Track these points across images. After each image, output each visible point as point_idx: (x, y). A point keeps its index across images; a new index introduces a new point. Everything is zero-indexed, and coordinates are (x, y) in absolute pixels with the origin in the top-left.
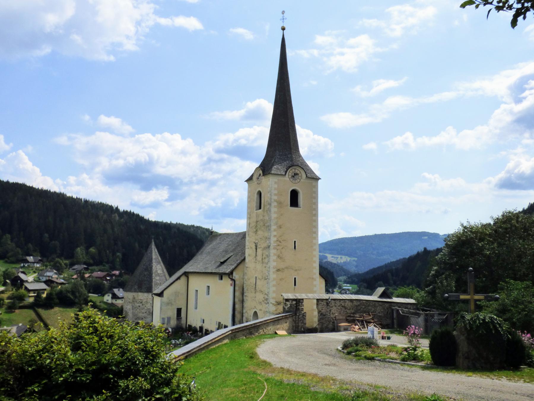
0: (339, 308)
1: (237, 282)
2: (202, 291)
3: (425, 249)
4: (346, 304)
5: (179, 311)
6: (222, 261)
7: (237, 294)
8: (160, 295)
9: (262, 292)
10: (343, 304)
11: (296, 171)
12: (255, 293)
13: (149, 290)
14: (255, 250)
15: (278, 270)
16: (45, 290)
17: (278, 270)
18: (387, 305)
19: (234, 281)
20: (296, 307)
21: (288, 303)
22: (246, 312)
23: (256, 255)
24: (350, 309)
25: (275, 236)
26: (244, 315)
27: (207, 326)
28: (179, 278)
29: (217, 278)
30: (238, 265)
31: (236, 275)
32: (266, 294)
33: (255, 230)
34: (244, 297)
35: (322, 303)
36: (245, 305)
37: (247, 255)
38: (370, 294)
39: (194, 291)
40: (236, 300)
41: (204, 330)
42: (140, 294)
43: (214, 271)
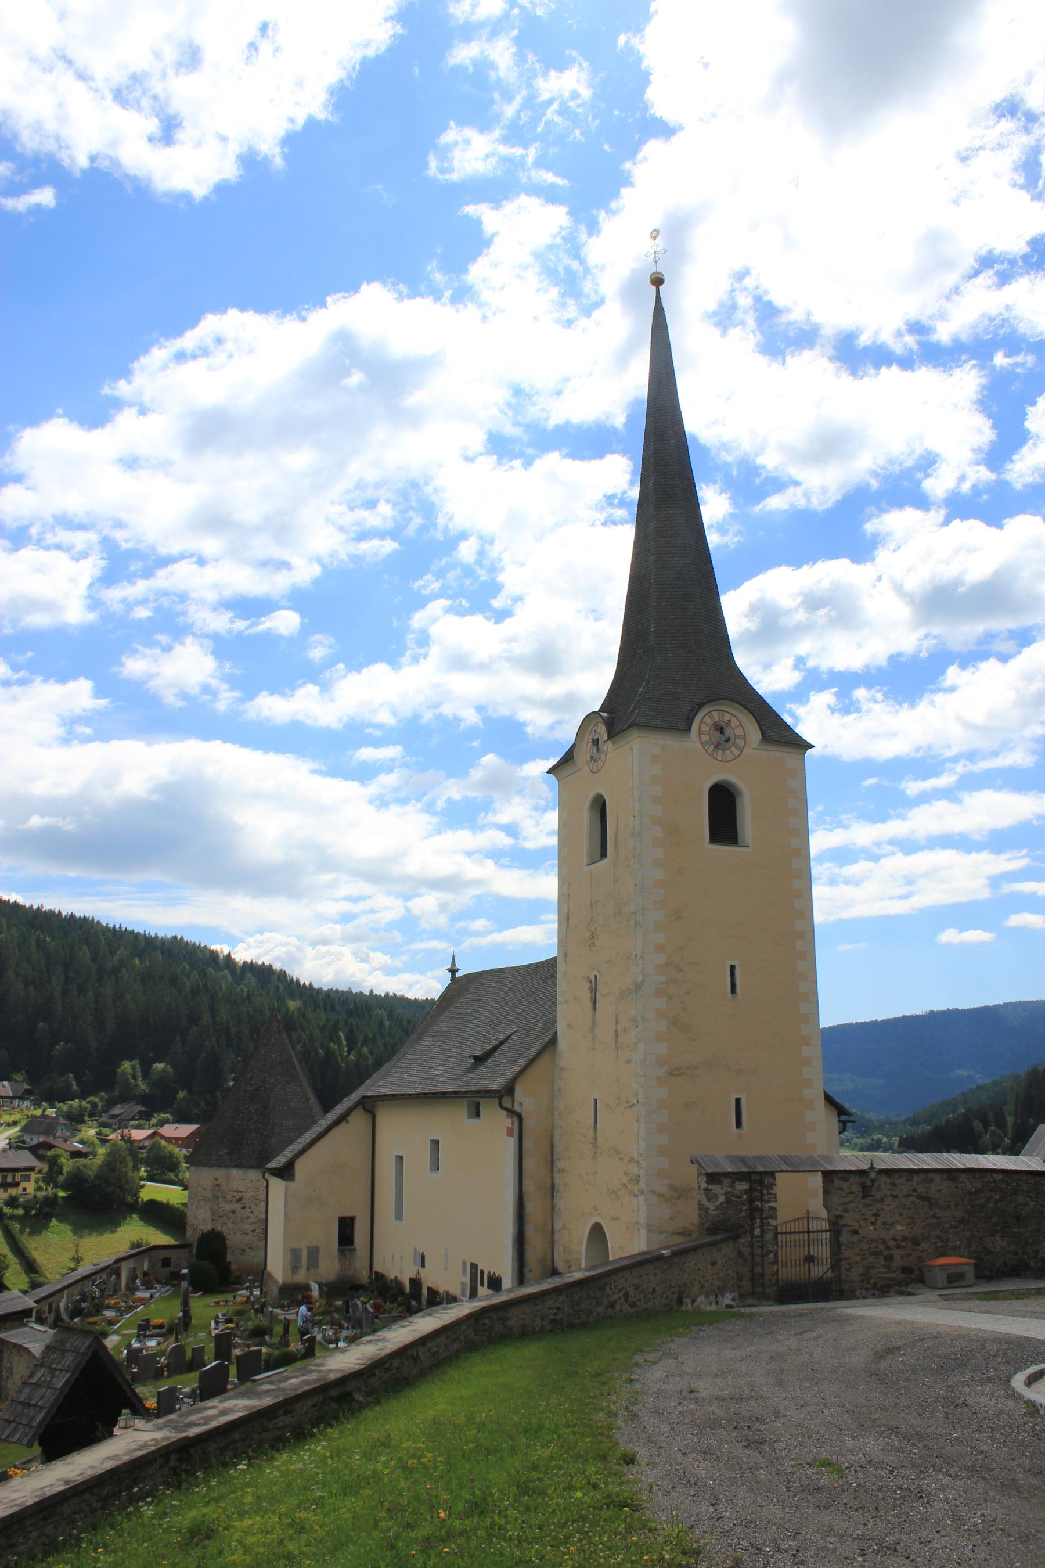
1: (528, 1123)
2: (418, 1158)
5: (346, 1226)
6: (478, 1052)
8: (286, 1172)
9: (617, 1152)
10: (921, 1189)
11: (727, 717)
12: (595, 1157)
13: (260, 1162)
14: (589, 1005)
17: (675, 1072)
19: (520, 1117)
20: (751, 1200)
21: (715, 1188)
22: (564, 1227)
23: (594, 1024)
24: (948, 1207)
25: (659, 948)
26: (557, 1236)
27: (434, 1278)
28: (343, 1118)
29: (460, 1112)
30: (532, 1061)
31: (524, 1098)
32: (631, 1160)
33: (588, 935)
34: (557, 1175)
35: (845, 1185)
36: (560, 1204)
37: (561, 1027)
38: (1014, 1150)
39: (393, 1160)
40: (529, 1186)
41: (425, 1291)
42: (235, 1172)
43: (451, 1089)
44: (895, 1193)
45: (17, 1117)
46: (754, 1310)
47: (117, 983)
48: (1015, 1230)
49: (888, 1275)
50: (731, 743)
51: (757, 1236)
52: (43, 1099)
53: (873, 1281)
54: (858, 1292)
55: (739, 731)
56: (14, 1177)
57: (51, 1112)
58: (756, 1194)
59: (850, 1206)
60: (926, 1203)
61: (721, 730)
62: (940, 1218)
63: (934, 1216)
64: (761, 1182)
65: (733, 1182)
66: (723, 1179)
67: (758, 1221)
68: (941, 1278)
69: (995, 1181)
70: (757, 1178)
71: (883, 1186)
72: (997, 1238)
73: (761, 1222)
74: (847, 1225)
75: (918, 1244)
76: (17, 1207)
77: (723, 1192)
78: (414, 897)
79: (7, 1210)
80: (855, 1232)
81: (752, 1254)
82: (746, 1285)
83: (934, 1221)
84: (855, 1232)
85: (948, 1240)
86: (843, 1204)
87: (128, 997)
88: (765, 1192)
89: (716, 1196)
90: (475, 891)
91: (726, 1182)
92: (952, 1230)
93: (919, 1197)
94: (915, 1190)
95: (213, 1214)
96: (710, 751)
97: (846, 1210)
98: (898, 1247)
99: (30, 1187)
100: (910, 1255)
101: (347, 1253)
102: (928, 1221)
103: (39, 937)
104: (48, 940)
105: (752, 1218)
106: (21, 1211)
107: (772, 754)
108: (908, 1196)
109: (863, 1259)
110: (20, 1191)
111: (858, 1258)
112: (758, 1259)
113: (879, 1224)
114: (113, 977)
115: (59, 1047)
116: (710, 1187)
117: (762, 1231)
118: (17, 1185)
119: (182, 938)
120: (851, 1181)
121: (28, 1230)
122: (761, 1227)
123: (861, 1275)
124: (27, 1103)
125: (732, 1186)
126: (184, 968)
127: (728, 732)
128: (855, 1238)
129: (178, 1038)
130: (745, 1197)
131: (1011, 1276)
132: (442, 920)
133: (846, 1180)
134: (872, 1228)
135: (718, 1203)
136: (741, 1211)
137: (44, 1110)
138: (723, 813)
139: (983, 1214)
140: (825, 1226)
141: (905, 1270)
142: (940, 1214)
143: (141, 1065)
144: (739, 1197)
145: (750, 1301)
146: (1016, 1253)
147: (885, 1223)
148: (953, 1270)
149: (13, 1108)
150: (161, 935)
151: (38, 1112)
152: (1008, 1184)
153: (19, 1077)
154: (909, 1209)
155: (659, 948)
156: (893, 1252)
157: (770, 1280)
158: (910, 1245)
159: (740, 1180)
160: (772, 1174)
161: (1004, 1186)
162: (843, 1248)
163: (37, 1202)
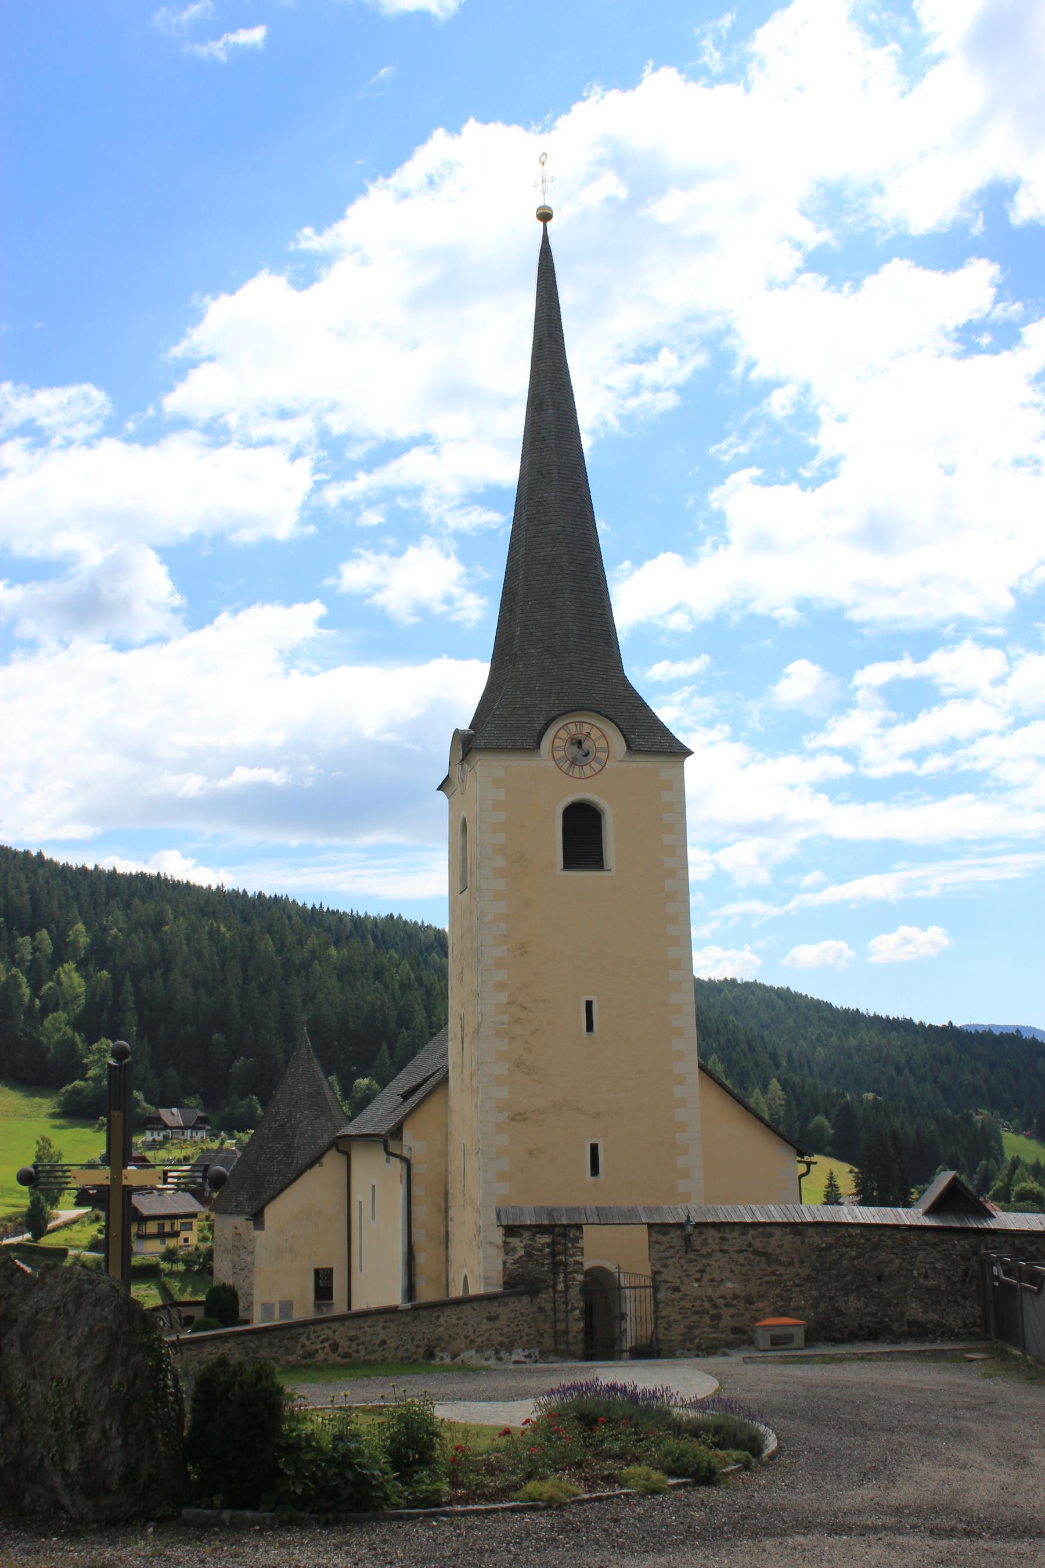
0: (741, 1258)
1: (418, 1169)
3: (950, 1023)
4: (773, 1241)
7: (420, 1212)
10: (758, 1244)
15: (518, 1117)
16: (194, 1215)
17: (518, 1117)
18: (964, 1244)
19: (407, 1162)
20: (554, 1254)
21: (514, 1241)
24: (790, 1264)
25: (501, 986)
31: (412, 1141)
40: (419, 1235)
44: (725, 1248)
45: (188, 1152)
46: (555, 1365)
47: (308, 980)
48: (876, 1290)
49: (715, 1335)
50: (590, 757)
51: (561, 1292)
52: (221, 1128)
53: (696, 1341)
54: (678, 1352)
55: (601, 743)
56: (172, 1225)
57: (230, 1144)
58: (559, 1248)
59: (670, 1262)
60: (763, 1259)
61: (580, 744)
62: (781, 1275)
63: (773, 1273)
64: (565, 1235)
65: (534, 1235)
66: (522, 1232)
67: (562, 1276)
68: (763, 1339)
69: (850, 1236)
70: (562, 1231)
71: (710, 1241)
72: (852, 1298)
73: (565, 1277)
74: (665, 1282)
75: (752, 1303)
76: (176, 1261)
77: (522, 1245)
78: (723, 846)
79: (165, 1266)
80: (677, 1289)
81: (554, 1310)
82: (548, 1342)
83: (774, 1278)
84: (677, 1289)
85: (791, 1299)
86: (661, 1259)
87: (321, 996)
88: (570, 1245)
89: (514, 1249)
90: (802, 835)
91: (527, 1235)
92: (796, 1289)
93: (755, 1252)
94: (750, 1245)
95: (234, 1266)
96: (564, 768)
97: (665, 1266)
98: (727, 1305)
99: (193, 1236)
100: (742, 1315)
101: (324, 1309)
102: (766, 1279)
103: (212, 927)
104: (223, 929)
105: (555, 1273)
106: (181, 1267)
107: (642, 765)
108: (741, 1251)
109: (685, 1318)
110: (181, 1242)
111: (679, 1317)
112: (561, 1316)
113: (705, 1280)
114: (303, 972)
115: (240, 1063)
116: (509, 1240)
117: (566, 1287)
118: (176, 1234)
119: (400, 917)
120: (671, 1235)
121: (190, 1289)
122: (565, 1281)
123: (682, 1335)
124: (202, 1134)
125: (532, 1239)
126: (391, 957)
127: (586, 745)
128: (676, 1296)
129: (385, 1046)
130: (547, 1250)
131: (868, 1340)
132: (764, 877)
133: (666, 1234)
134: (696, 1285)
135: (517, 1256)
136: (543, 1265)
137: (222, 1143)
138: (583, 836)
139: (835, 1272)
140: (648, 1282)
141: (736, 1330)
142: (781, 1271)
143: (340, 1082)
144: (541, 1250)
145: (552, 1358)
146: (875, 1315)
147: (712, 1280)
148: (778, 1332)
149: (185, 1141)
150: (373, 913)
151: (215, 1145)
152: (867, 1239)
153: (192, 1101)
154: (742, 1265)
155: (501, 986)
156: (720, 1311)
157: (575, 1337)
158: (742, 1304)
159: (542, 1233)
160: (579, 1227)
161: (862, 1241)
162: (661, 1305)
163: (199, 1256)
